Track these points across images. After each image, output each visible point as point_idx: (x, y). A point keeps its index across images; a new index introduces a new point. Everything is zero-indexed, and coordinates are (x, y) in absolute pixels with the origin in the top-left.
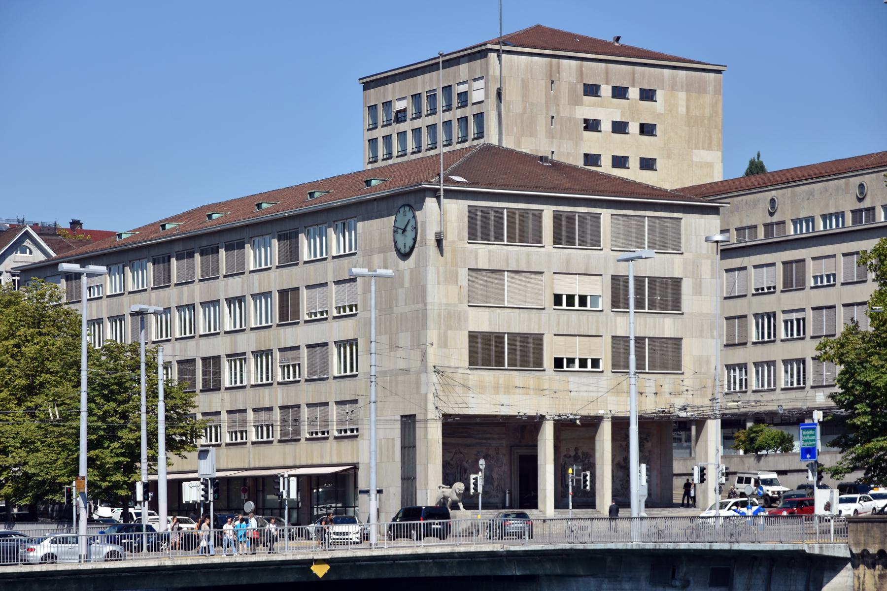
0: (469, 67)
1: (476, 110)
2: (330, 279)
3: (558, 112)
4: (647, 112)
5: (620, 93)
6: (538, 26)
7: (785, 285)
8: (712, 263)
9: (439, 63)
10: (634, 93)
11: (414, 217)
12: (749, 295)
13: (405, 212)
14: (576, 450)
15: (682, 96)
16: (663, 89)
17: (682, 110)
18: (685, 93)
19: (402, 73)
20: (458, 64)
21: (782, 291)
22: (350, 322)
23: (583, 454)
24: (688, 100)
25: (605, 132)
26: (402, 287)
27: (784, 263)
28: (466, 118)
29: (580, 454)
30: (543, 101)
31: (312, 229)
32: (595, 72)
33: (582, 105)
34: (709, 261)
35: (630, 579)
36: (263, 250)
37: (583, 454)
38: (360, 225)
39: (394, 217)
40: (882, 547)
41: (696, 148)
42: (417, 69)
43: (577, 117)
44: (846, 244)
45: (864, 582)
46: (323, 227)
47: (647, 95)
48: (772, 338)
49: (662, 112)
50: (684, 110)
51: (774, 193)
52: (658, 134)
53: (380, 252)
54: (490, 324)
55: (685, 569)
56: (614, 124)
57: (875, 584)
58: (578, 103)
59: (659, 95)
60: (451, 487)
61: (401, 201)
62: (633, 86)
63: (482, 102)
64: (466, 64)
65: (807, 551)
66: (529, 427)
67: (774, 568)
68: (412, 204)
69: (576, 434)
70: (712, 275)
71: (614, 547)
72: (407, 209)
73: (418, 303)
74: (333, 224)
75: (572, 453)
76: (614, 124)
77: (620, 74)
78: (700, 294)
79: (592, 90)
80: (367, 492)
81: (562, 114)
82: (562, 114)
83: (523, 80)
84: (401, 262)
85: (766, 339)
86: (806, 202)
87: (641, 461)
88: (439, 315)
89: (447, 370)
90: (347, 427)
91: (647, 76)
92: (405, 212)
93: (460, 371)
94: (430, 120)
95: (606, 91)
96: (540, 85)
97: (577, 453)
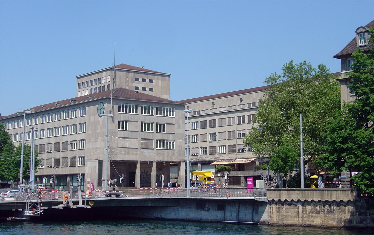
0: (106, 73)
1: (103, 85)
2: (78, 123)
3: (129, 85)
4: (151, 85)
5: (144, 80)
6: (123, 64)
7: (238, 123)
8: (183, 120)
9: (112, 68)
10: (148, 80)
11: (104, 105)
12: (191, 130)
13: (101, 104)
14: (144, 170)
15: (160, 81)
16: (155, 79)
17: (160, 85)
18: (160, 81)
19: (88, 75)
20: (103, 72)
21: (200, 129)
22: (84, 134)
23: (146, 172)
24: (161, 82)
25: (141, 90)
26: (99, 124)
27: (248, 115)
28: (105, 86)
29: (145, 172)
30: (125, 82)
31: (42, 116)
32: (138, 76)
33: (135, 83)
34: (182, 120)
35: (188, 208)
36: (17, 123)
37: (146, 172)
38: (87, 108)
39: (98, 105)
40: (279, 199)
41: (163, 95)
42: (92, 74)
43: (133, 86)
44: (210, 117)
45: (272, 210)
46: (31, 118)
47: (151, 81)
48: (197, 141)
49: (155, 85)
50: (160, 85)
51: (241, 96)
52: (153, 91)
53: (93, 115)
54: (124, 135)
55: (208, 205)
56: (143, 88)
57: (277, 210)
58: (134, 82)
59: (154, 81)
60: (113, 180)
61: (100, 102)
62: (148, 79)
63: (109, 82)
64: (105, 72)
65: (255, 200)
66: (133, 164)
67: (240, 205)
68: (103, 102)
69: (146, 165)
70: (183, 123)
71: (177, 198)
72: (102, 103)
73: (104, 129)
74: (14, 121)
75: (143, 171)
76: (143, 88)
77: (144, 76)
78: (180, 128)
79: (137, 79)
80: (104, 180)
81: (130, 85)
82: (130, 85)
83: (120, 76)
84: (99, 118)
85: (195, 142)
86: (197, 107)
87: (196, 171)
88: (110, 132)
89: (112, 147)
90: (49, 165)
91: (151, 77)
92: (101, 104)
93: (115, 148)
94: (95, 87)
95: (141, 80)
96: (125, 78)
97: (145, 171)
